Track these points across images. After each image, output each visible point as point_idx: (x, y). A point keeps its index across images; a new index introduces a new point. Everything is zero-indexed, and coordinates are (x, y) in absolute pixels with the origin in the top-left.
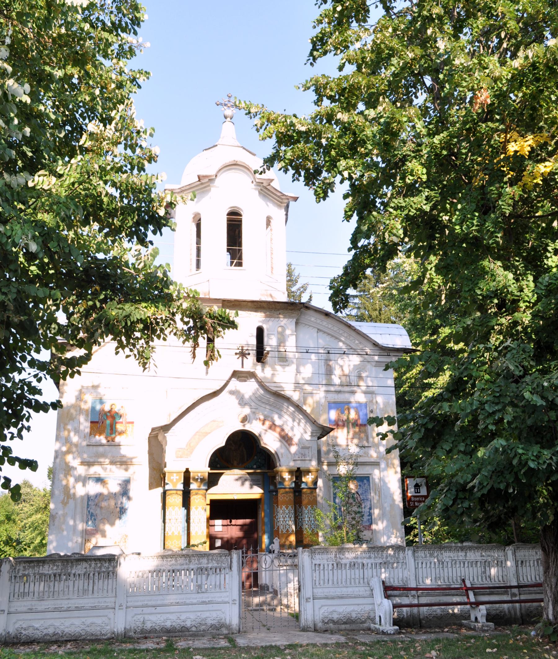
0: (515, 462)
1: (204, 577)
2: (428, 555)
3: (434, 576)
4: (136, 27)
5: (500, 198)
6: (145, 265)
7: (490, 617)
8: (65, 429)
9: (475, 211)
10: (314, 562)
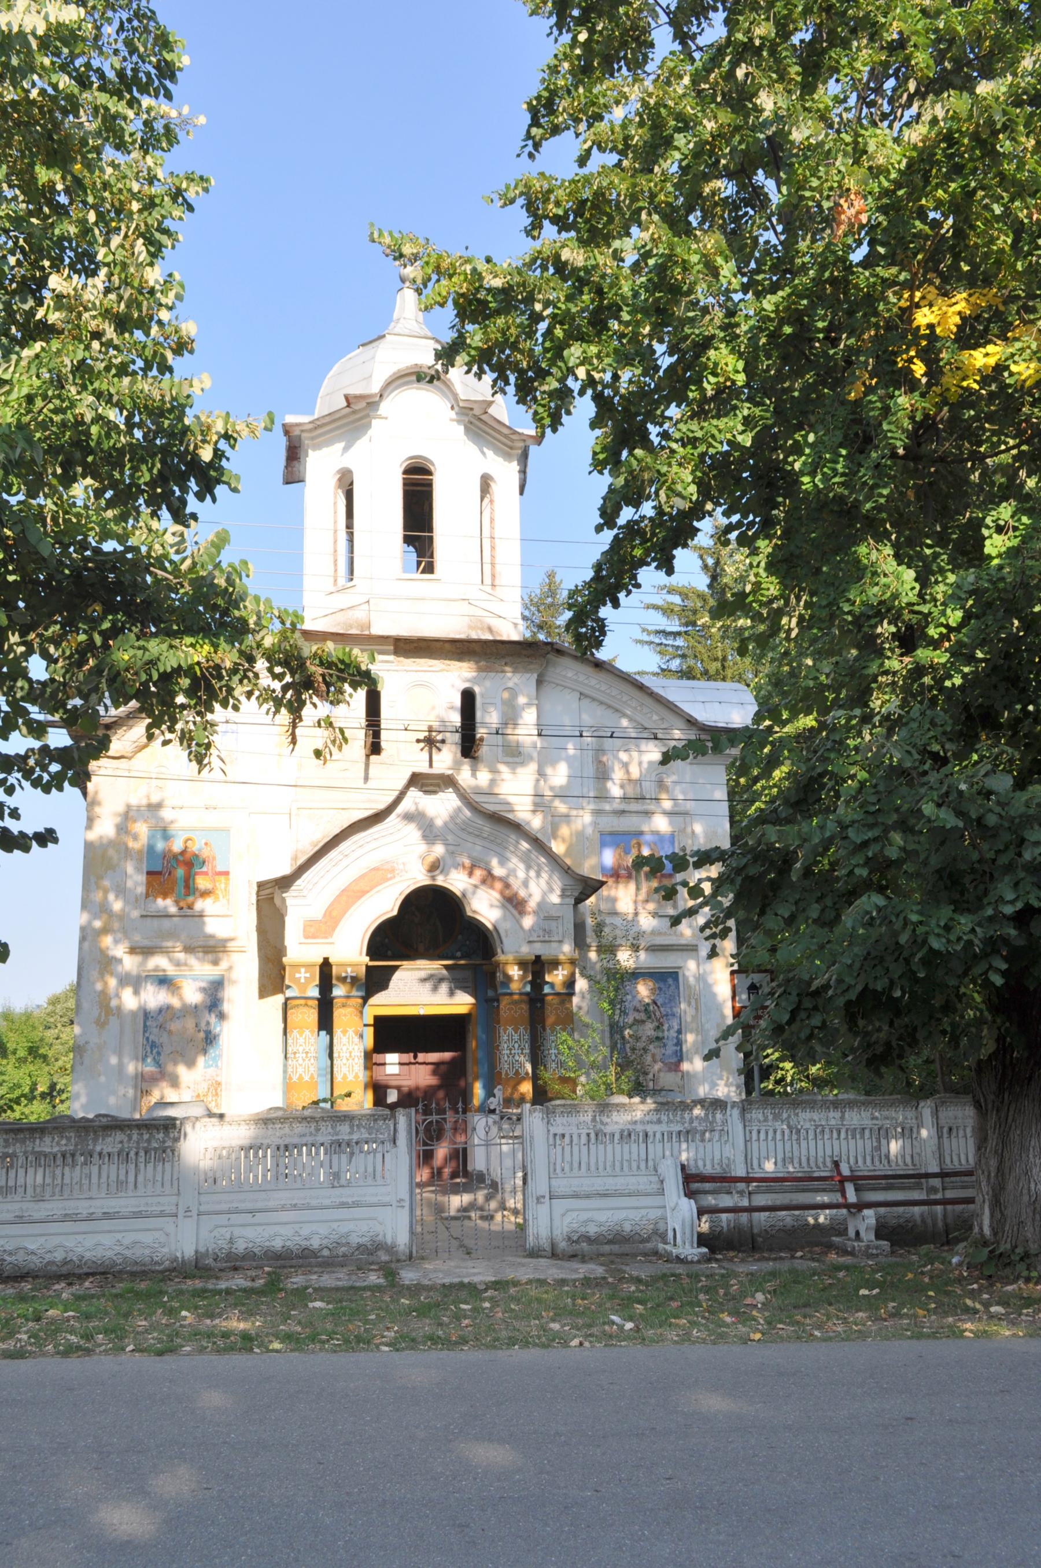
0: (903, 939)
1: (344, 1158)
2: (770, 1117)
3: (780, 1156)
4: (167, 83)
5: (886, 418)
6: (194, 564)
7: (882, 1231)
8: (98, 887)
9: (841, 445)
10: (553, 1130)
